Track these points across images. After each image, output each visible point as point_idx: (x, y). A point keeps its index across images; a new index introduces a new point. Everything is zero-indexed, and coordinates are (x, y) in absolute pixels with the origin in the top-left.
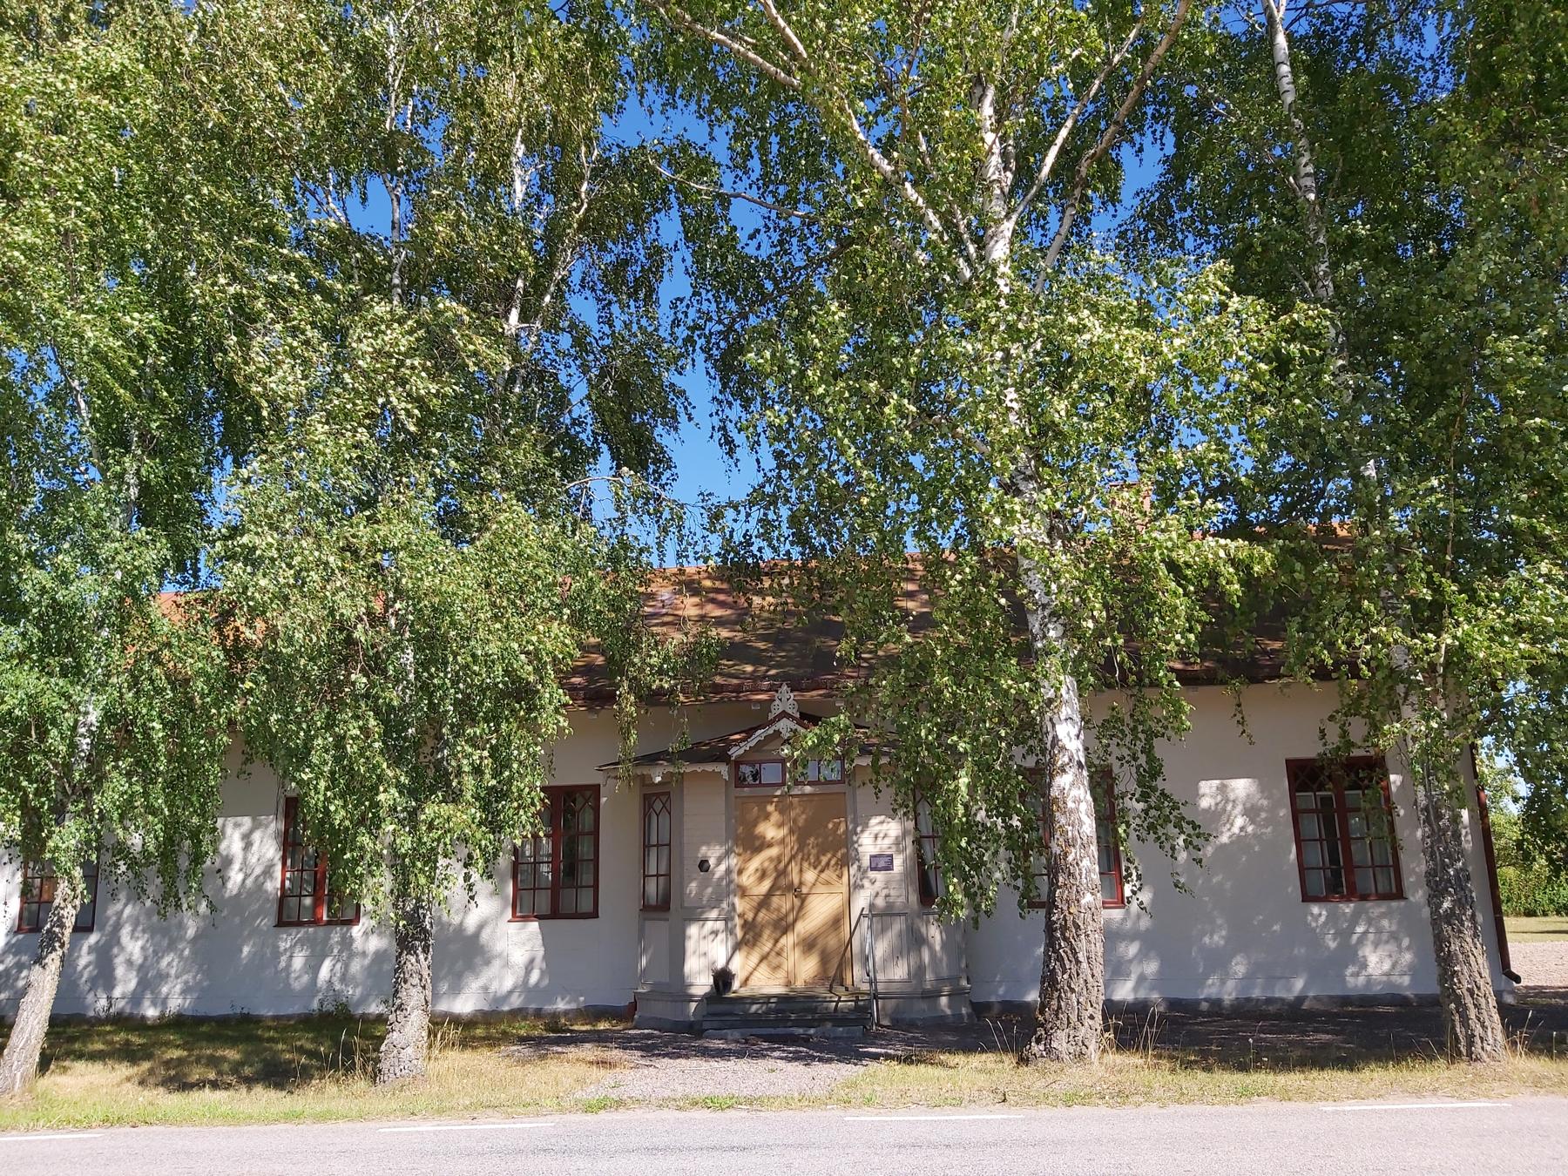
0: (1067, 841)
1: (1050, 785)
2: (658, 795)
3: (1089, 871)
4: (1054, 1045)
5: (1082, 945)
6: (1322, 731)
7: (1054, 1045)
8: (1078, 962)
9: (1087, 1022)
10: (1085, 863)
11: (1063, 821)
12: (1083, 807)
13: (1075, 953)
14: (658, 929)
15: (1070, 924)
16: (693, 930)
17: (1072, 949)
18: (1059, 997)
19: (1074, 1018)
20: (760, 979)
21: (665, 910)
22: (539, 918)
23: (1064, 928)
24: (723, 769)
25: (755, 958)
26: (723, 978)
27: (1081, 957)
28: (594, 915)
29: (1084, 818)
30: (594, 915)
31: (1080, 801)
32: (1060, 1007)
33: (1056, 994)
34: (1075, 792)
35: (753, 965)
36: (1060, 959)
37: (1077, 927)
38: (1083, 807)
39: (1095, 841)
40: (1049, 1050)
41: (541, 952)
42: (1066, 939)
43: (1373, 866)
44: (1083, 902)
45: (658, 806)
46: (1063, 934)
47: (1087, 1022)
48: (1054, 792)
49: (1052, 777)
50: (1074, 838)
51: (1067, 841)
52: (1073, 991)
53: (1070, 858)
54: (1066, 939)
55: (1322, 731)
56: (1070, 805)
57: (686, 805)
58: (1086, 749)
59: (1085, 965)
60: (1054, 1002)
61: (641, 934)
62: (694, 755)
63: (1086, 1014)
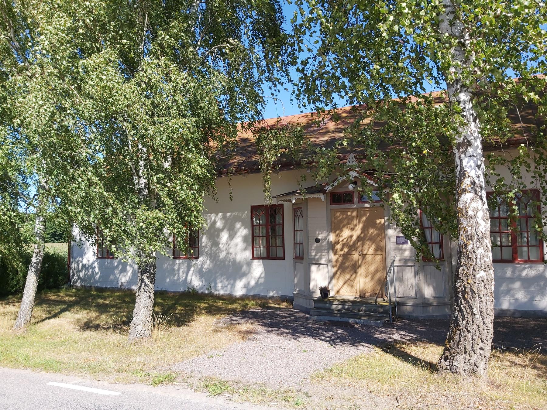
0: (467, 237)
1: (458, 200)
2: (298, 208)
3: (482, 257)
4: (455, 363)
5: (476, 304)
6: (285, 89)
7: (455, 363)
8: (473, 314)
9: (478, 351)
10: (480, 251)
11: (465, 224)
12: (480, 214)
13: (471, 309)
14: (300, 266)
15: (468, 290)
16: (314, 268)
17: (469, 305)
18: (460, 334)
19: (469, 349)
20: (345, 291)
21: (303, 260)
22: (259, 258)
23: (464, 292)
24: (322, 196)
25: (341, 282)
26: (325, 292)
27: (475, 311)
28: (283, 258)
29: (480, 221)
30: (283, 258)
31: (478, 210)
32: (460, 341)
33: (458, 332)
34: (474, 205)
35: (341, 286)
36: (461, 311)
37: (473, 292)
38: (480, 214)
39: (488, 236)
40: (451, 366)
41: (263, 275)
42: (465, 299)
43: (432, 243)
44: (478, 276)
45: (299, 213)
46: (463, 295)
47: (478, 351)
48: (460, 205)
49: (459, 195)
50: (472, 235)
51: (467, 237)
52: (469, 332)
53: (469, 248)
54: (465, 299)
55: (285, 89)
56: (470, 213)
57: (309, 213)
58: (485, 175)
59: (478, 316)
60: (457, 337)
61: (295, 269)
62: (310, 190)
63: (477, 348)
